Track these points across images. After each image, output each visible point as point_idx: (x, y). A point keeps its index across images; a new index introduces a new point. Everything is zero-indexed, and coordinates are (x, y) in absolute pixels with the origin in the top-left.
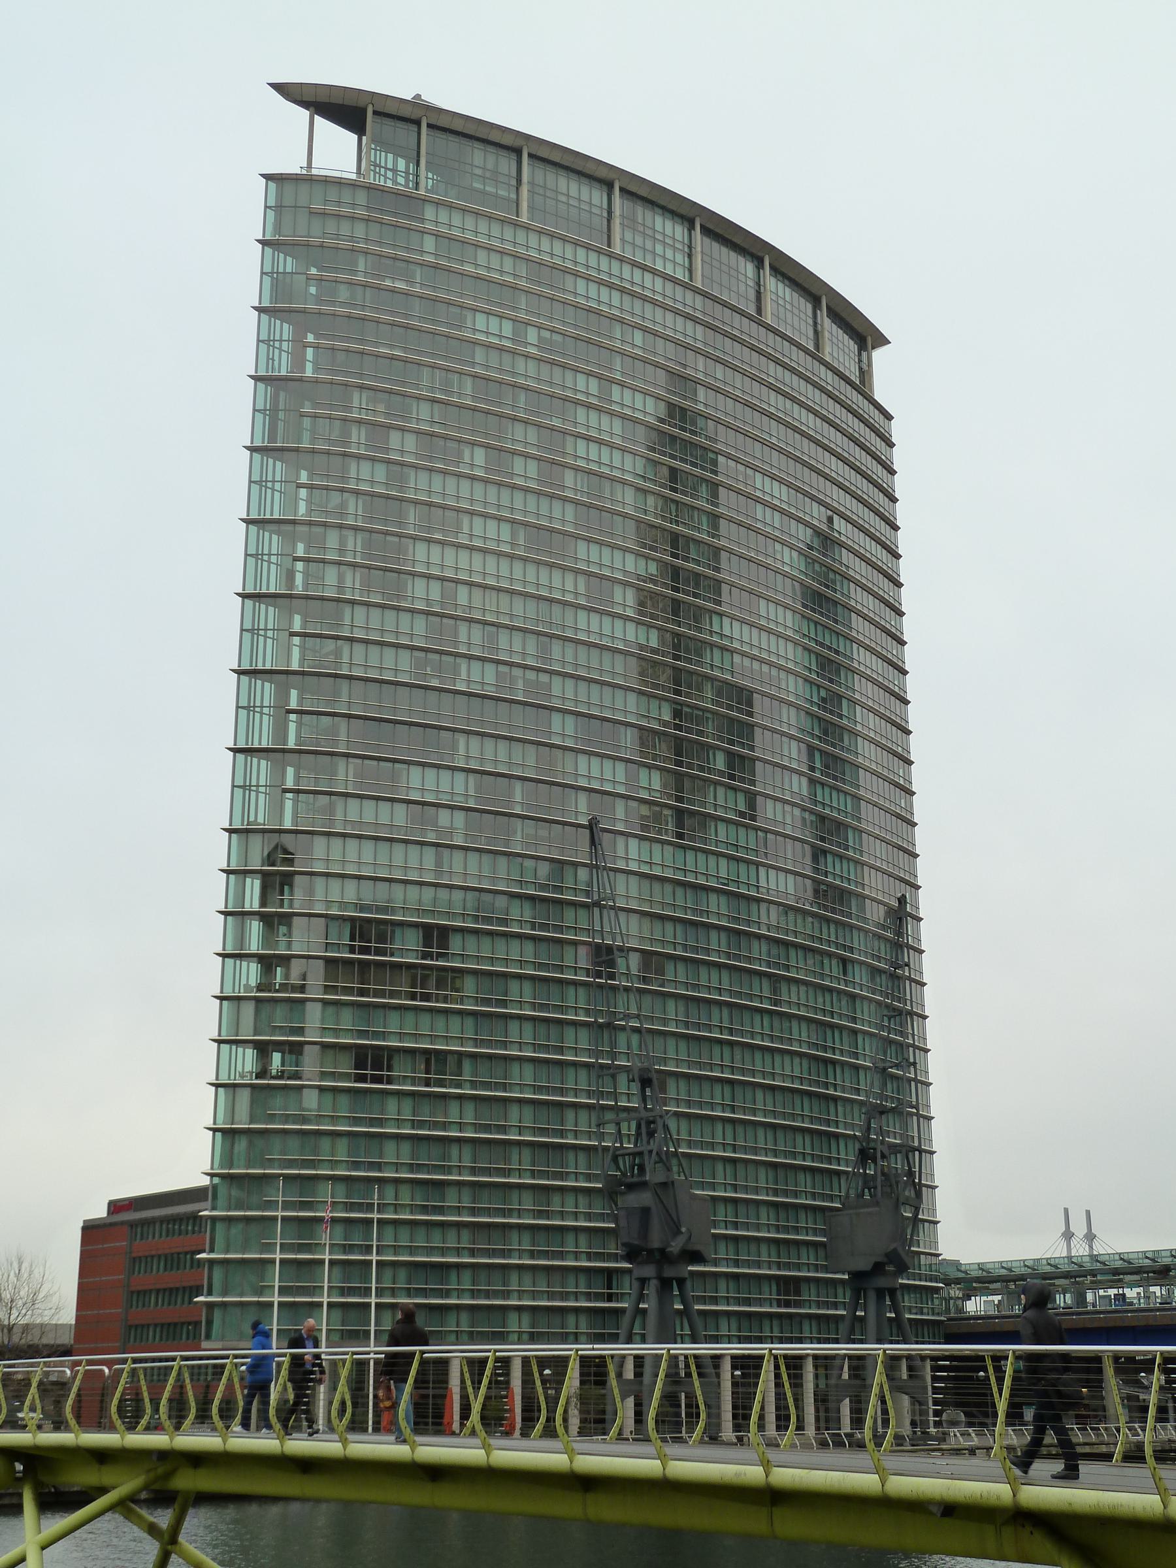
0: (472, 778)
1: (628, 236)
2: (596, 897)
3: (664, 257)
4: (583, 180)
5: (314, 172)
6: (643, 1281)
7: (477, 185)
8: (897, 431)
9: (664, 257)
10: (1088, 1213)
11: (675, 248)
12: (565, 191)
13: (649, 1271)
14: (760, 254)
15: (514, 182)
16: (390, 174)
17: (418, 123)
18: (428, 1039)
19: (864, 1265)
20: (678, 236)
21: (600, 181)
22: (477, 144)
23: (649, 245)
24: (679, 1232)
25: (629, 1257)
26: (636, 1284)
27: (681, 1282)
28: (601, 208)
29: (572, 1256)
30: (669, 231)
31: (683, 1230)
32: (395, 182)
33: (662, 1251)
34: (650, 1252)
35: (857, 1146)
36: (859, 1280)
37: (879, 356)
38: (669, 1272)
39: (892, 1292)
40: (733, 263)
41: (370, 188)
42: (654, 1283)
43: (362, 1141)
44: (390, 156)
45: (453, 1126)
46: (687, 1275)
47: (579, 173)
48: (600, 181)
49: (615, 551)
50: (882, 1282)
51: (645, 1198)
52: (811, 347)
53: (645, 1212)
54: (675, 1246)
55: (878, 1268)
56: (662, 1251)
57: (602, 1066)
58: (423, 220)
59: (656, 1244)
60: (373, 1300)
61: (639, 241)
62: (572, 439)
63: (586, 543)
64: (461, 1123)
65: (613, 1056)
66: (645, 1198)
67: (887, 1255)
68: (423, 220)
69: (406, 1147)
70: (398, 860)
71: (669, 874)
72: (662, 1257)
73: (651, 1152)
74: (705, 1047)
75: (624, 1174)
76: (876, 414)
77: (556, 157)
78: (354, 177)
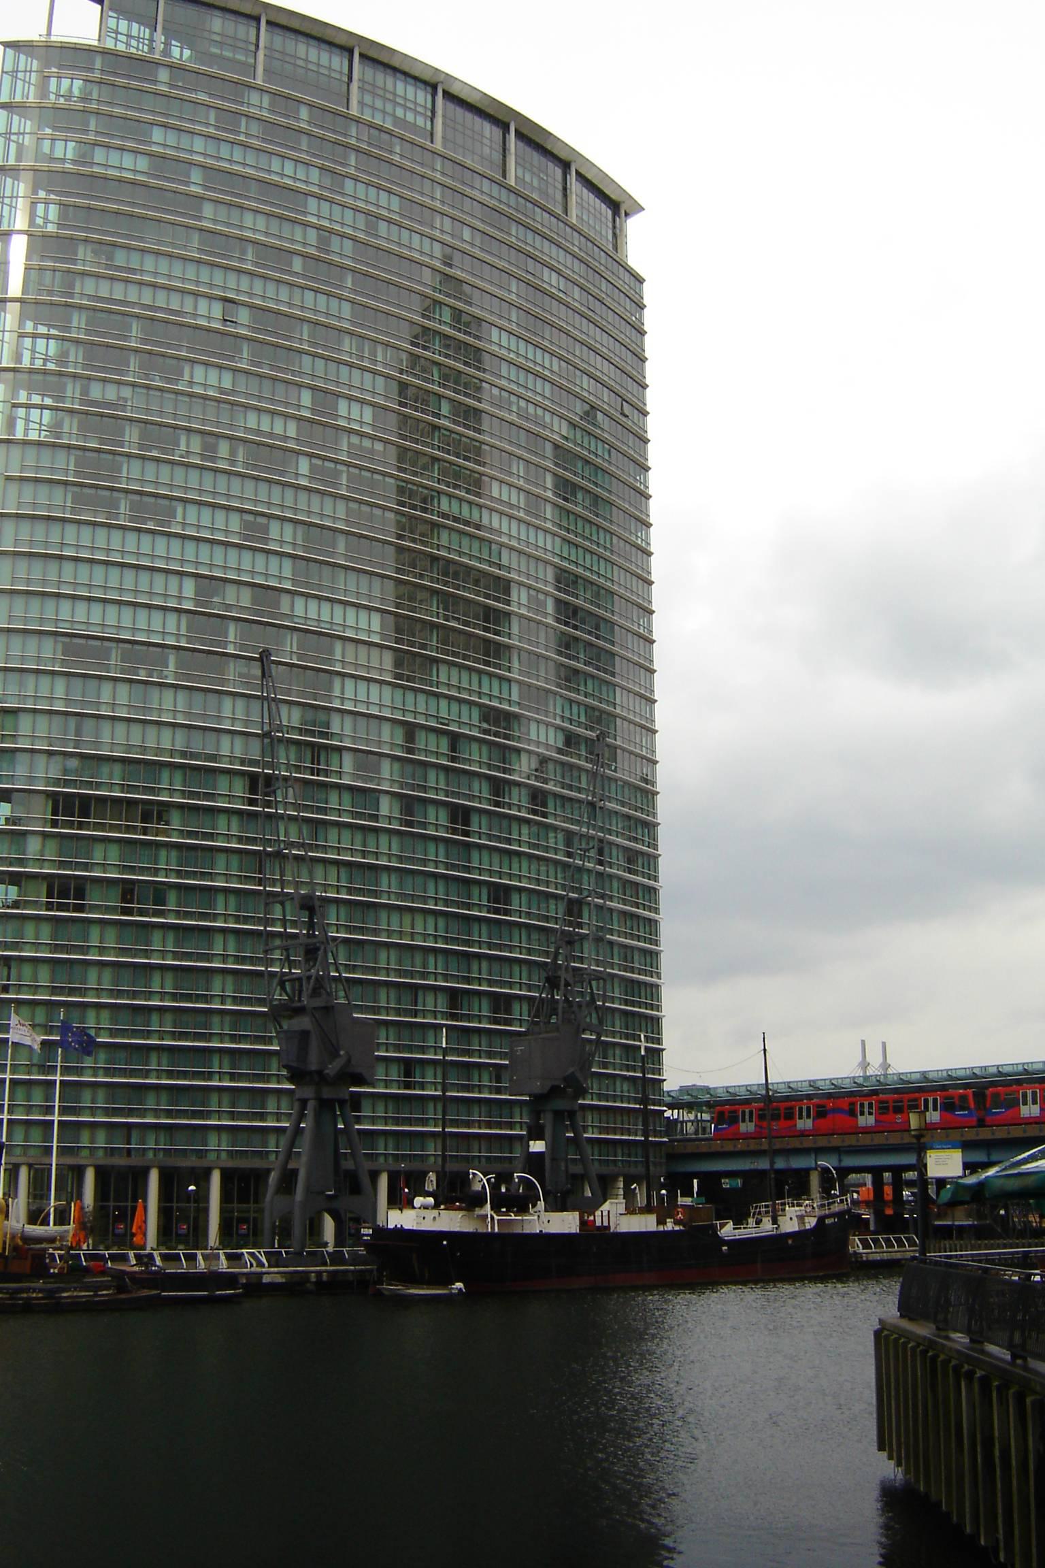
0: (184, 619)
1: (368, 99)
2: (266, 728)
3: (384, 112)
4: (323, 46)
5: (53, 38)
6: (304, 1103)
7: (215, 50)
8: (649, 294)
9: (384, 112)
10: (884, 1044)
11: (416, 112)
12: (327, 64)
13: (308, 1092)
14: (506, 120)
15: (253, 48)
16: (134, 43)
17: (257, 19)
18: (223, 878)
19: (538, 1086)
20: (421, 100)
21: (342, 48)
22: (217, 13)
23: (389, 108)
24: (337, 1055)
25: (291, 1079)
26: (297, 1105)
27: (571, 1114)
28: (341, 72)
29: (90, 1072)
30: (410, 96)
31: (342, 1053)
32: (128, 45)
33: (320, 1073)
34: (311, 1073)
35: (544, 975)
36: (538, 1103)
37: (634, 227)
38: (327, 1093)
39: (571, 1114)
40: (477, 128)
41: (105, 52)
42: (311, 1104)
43: (246, 980)
44: (147, 30)
45: (155, 954)
46: (577, 1108)
47: (331, 44)
48: (342, 48)
49: (353, 403)
50: (561, 1104)
51: (304, 1023)
52: (559, 211)
53: (304, 1035)
54: (332, 1069)
55: (554, 1092)
56: (320, 1073)
57: (270, 894)
58: (155, 82)
59: (313, 1067)
60: (56, 1118)
61: (379, 104)
62: (299, 290)
63: (359, 405)
64: (162, 951)
65: (283, 884)
66: (304, 1023)
67: (565, 1079)
68: (155, 82)
69: (107, 974)
70: (106, 697)
71: (386, 713)
72: (320, 1078)
73: (309, 978)
74: (419, 880)
75: (291, 999)
76: (627, 277)
77: (295, 24)
78: (96, 43)
